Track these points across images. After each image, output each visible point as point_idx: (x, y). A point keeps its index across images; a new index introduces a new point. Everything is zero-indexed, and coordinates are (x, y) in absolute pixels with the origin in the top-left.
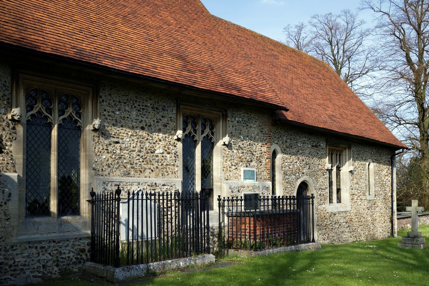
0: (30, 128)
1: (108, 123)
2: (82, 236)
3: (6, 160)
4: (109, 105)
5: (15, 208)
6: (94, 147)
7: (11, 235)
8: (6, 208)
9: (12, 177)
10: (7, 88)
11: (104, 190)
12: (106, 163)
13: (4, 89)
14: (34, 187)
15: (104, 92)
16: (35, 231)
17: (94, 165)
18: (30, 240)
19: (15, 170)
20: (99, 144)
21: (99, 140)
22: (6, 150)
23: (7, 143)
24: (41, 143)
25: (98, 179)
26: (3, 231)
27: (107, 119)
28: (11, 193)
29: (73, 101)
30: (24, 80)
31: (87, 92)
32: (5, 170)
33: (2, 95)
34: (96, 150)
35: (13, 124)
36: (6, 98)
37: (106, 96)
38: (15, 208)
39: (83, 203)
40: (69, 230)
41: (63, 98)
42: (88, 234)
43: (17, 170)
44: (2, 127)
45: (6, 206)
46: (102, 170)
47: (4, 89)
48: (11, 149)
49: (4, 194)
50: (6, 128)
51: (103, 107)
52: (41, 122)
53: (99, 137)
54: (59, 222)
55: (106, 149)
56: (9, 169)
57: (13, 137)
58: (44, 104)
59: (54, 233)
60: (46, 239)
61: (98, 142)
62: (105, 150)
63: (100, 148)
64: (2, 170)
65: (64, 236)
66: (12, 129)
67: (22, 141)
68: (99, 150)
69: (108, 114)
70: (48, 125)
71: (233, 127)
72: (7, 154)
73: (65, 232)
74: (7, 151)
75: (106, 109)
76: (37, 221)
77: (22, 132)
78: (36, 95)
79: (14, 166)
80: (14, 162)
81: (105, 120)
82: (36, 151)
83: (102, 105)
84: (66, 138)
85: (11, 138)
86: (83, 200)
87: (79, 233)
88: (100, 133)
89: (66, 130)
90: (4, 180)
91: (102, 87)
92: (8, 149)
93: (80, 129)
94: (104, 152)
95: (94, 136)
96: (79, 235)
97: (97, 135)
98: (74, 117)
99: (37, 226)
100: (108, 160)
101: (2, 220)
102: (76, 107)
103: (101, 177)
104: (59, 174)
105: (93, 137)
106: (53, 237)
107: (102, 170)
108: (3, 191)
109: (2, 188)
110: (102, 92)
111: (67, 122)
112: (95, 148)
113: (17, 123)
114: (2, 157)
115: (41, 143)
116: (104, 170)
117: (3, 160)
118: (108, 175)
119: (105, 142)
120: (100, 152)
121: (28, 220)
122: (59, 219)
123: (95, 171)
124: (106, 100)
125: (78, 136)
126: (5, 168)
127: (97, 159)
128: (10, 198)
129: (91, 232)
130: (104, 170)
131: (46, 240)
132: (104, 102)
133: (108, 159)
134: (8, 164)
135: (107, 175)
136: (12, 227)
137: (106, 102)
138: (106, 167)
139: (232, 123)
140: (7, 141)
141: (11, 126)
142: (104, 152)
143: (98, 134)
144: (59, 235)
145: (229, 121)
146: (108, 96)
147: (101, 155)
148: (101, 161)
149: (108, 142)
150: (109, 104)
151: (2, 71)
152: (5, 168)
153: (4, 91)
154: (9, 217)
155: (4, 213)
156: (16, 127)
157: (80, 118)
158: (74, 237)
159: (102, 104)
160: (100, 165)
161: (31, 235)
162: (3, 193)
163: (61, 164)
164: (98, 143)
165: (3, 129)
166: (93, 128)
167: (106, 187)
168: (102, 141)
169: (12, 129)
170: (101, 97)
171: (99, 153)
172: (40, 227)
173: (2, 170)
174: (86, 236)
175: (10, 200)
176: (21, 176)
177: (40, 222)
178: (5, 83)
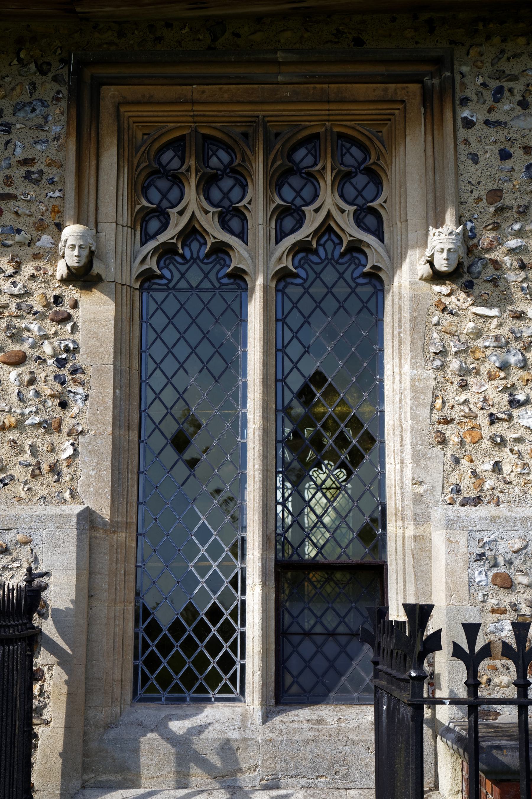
31: (401, 106)
58: (216, 195)
71: (505, 155)
139: (494, 134)
145: (469, 124)
157: (379, 235)
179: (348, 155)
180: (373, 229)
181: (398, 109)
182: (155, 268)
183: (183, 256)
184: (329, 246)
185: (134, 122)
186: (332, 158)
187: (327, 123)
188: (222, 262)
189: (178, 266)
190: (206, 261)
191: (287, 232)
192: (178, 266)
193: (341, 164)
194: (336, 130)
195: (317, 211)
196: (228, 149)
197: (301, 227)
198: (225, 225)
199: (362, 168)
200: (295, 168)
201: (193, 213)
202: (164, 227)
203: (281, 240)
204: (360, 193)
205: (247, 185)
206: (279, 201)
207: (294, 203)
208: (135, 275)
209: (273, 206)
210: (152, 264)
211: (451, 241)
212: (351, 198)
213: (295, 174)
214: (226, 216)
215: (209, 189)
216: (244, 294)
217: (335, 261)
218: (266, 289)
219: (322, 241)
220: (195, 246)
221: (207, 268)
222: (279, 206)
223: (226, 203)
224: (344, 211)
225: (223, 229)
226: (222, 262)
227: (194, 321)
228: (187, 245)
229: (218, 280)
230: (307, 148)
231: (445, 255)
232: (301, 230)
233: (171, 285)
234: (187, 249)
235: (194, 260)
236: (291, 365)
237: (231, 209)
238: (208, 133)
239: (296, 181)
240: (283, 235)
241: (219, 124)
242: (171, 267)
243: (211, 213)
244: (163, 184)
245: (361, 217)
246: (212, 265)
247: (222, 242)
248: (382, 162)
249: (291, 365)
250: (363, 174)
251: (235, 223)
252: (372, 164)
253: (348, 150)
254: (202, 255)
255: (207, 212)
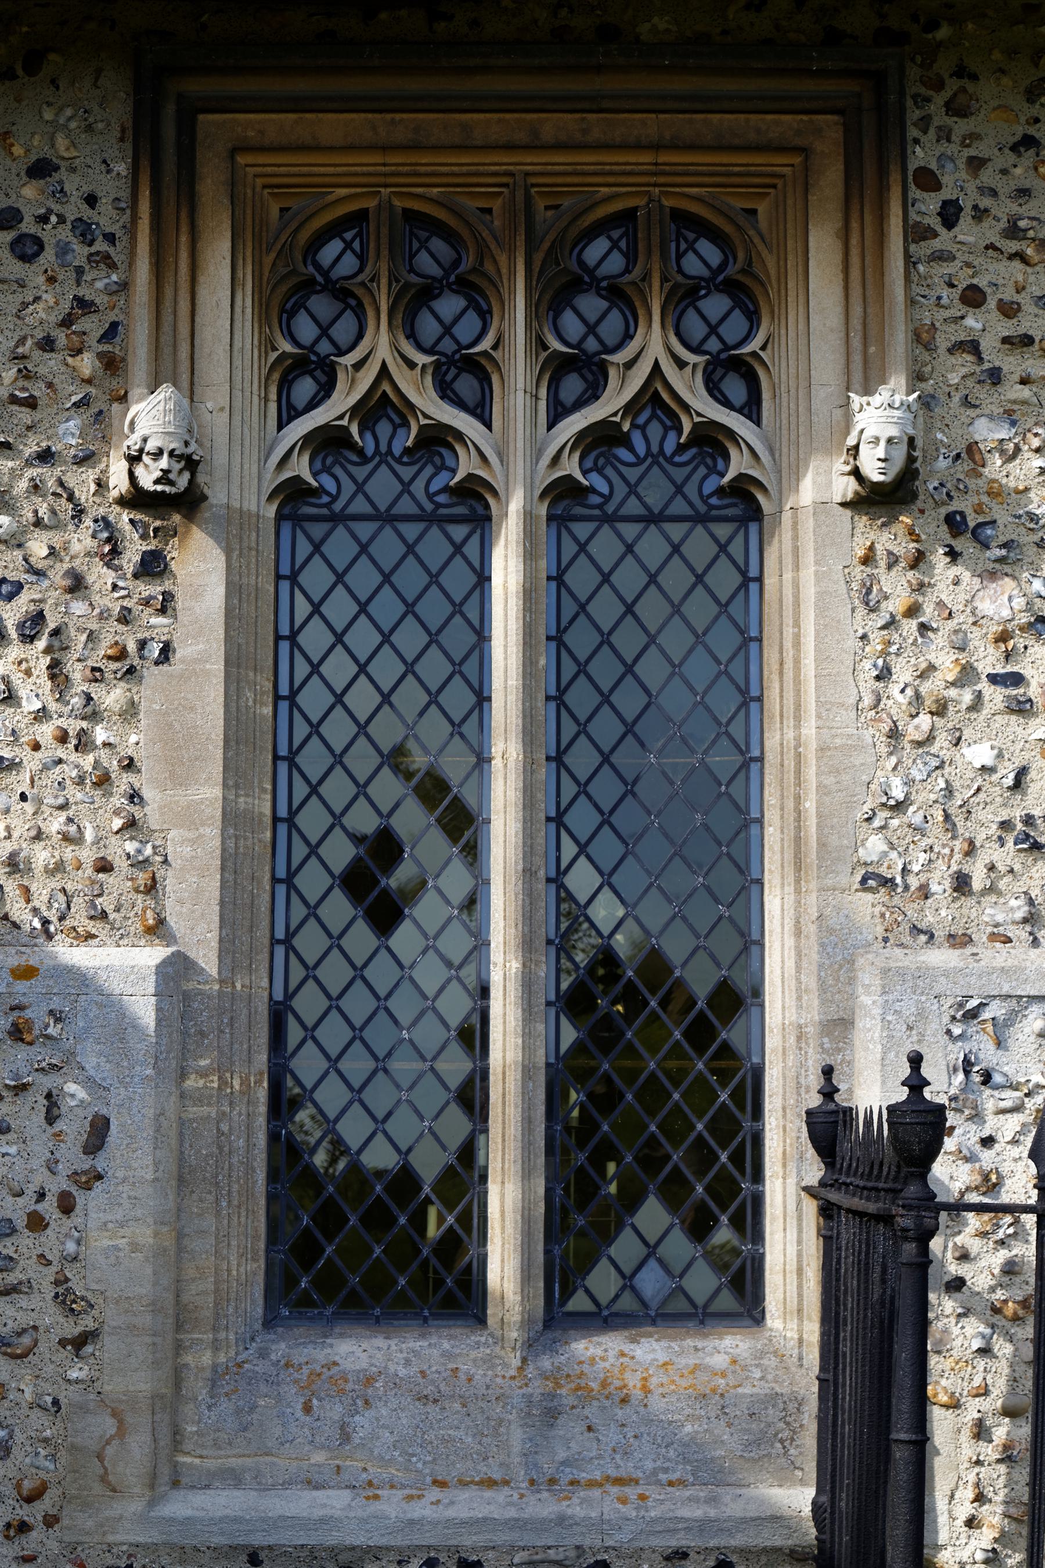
0: (317, 548)
1: (1010, 417)
2: (738, 1541)
3: (89, 835)
4: (1013, 246)
5: (135, 1247)
6: (868, 670)
7: (104, 1479)
8: (71, 1247)
9: (116, 986)
10: (101, 246)
11: (965, 1088)
12: (1004, 815)
13: (80, 261)
14: (441, 1066)
15: (961, 127)
16: (319, 1457)
17: (874, 846)
18: (258, 1540)
19: (161, 922)
20: (924, 628)
21: (921, 587)
22: (90, 758)
23: (97, 691)
24: (410, 668)
25: (902, 973)
26: (46, 1440)
27: (995, 377)
28: (107, 1121)
29: (692, 265)
30: (241, 160)
31: (797, 160)
32: (79, 918)
33: (66, 306)
34: (897, 699)
35: (144, 537)
36: (92, 326)
37: (976, 164)
38: (135, 1247)
39: (779, 1212)
40: (627, 1469)
41: (595, 251)
42: (777, 1520)
43: (172, 921)
44: (66, 566)
45: (68, 1223)
46: (961, 884)
47: (80, 261)
48: (133, 739)
49: (60, 1125)
50: (100, 576)
51: (947, 269)
52: (406, 487)
53: (918, 560)
54: (537, 1388)
55: (993, 679)
56: (109, 909)
57: (142, 644)
58: (695, 328)
59: (490, 1483)
60: (398, 1541)
61: (913, 611)
62: (984, 686)
63: (932, 668)
64: (61, 919)
65: (561, 1520)
66: (136, 576)
67: (218, 667)
68: (925, 688)
69: (1006, 328)
70: (461, 510)
72: (97, 785)
73: (592, 1484)
74: (97, 764)
75: (982, 282)
76: (347, 1365)
77: (221, 590)
78: (631, 257)
79: (152, 888)
80: (148, 851)
81: (981, 393)
82: (362, 740)
83: (941, 257)
84: (629, 609)
85: (132, 647)
86: (779, 1183)
87: (713, 1500)
88: (932, 526)
89: (630, 530)
90: (56, 1004)
91: (939, 86)
92: (106, 745)
93: (755, 513)
94: (976, 706)
95: (868, 560)
96: (703, 1526)
97: (905, 548)
98: (686, 407)
99: (335, 1411)
100: (1018, 785)
101: (42, 1347)
102: (714, 317)
103: (942, 957)
104: (469, 943)
105: (859, 572)
106: (463, 1523)
107: (961, 884)
108: (49, 1096)
109: (40, 1078)
110: (945, 135)
111: (640, 461)
112: (884, 675)
113: (177, 518)
114: (62, 817)
115: (410, 668)
116: (977, 885)
117: (66, 838)
118: (1021, 933)
119: (985, 606)
120: (940, 710)
121: (280, 1349)
122: (546, 1363)
123: (882, 894)
124: (985, 202)
125: (744, 573)
126: (79, 904)
127: (909, 782)
128: (100, 1163)
129: (815, 1504)
130: (978, 883)
131: (399, 1550)
132: (965, 221)
133: (1022, 773)
134: (104, 867)
135: (1012, 932)
136: (114, 1414)
137: (980, 214)
138: (1006, 855)
140: (96, 675)
141: (134, 549)
142: (976, 706)
143: (911, 532)
144: (512, 1513)
146: (1011, 157)
147: (942, 743)
148: (949, 791)
149: (1019, 603)
150: (1013, 231)
151: (73, 125)
152: (79, 904)
153: (80, 271)
154: (88, 1323)
155: (57, 1283)
156: (173, 551)
157: (752, 410)
158: (656, 1542)
159: (944, 240)
160: (936, 834)
161: (287, 1484)
162: (51, 1119)
163: (583, 849)
164: (910, 626)
165: (67, 582)
166: (849, 487)
167: (987, 1053)
168: (955, 599)
169: (136, 576)
170: (928, 180)
171: (924, 721)
172: (363, 1423)
173: (61, 919)
174: (778, 1542)
175: (99, 1177)
176: (208, 960)
177: (369, 1381)
178: (86, 212)
179: (690, 255)
180: (471, 404)
181: (792, 165)
182: (578, 476)
183: (360, 452)
184: (655, 430)
185: (265, 187)
186: (392, 257)
187: (382, 190)
188: (437, 460)
189: (349, 467)
190: (405, 459)
191: (300, 406)
192: (349, 467)
193: (409, 272)
194: (667, 203)
195: (358, 366)
196: (717, 237)
197: (328, 395)
198: (446, 391)
199: (721, 278)
200: (587, 279)
201: (656, 362)
202: (326, 389)
203: (288, 422)
204: (713, 330)
205: (490, 312)
206: (287, 347)
207: (584, 346)
208: (268, 487)
209: (273, 356)
210: (301, 467)
211: (884, 419)
212: (428, 342)
213: (587, 291)
214: (448, 370)
215: (415, 315)
216: (487, 524)
217: (666, 458)
218: (528, 516)
219: (641, 420)
220: (384, 429)
221: (679, 474)
222: (284, 355)
223: (447, 346)
224: (687, 364)
225: (442, 398)
226: (437, 460)
227: (699, 579)
228: (368, 428)
229: (430, 497)
230: (610, 238)
231: (880, 451)
232: (329, 402)
233: (610, 509)
234: (369, 436)
235: (384, 457)
236: (465, 668)
237: (457, 356)
238: (416, 208)
239: (321, 305)
240: (560, 409)
241: (436, 190)
242: (338, 471)
243: (690, 367)
244: (321, 305)
245: (449, 377)
246: (416, 468)
247: (713, 423)
248: (489, 267)
249: (465, 668)
250: (453, 291)
251: (466, 385)
252: (470, 272)
253: (691, 247)
254: (397, 451)
255: (411, 365)
